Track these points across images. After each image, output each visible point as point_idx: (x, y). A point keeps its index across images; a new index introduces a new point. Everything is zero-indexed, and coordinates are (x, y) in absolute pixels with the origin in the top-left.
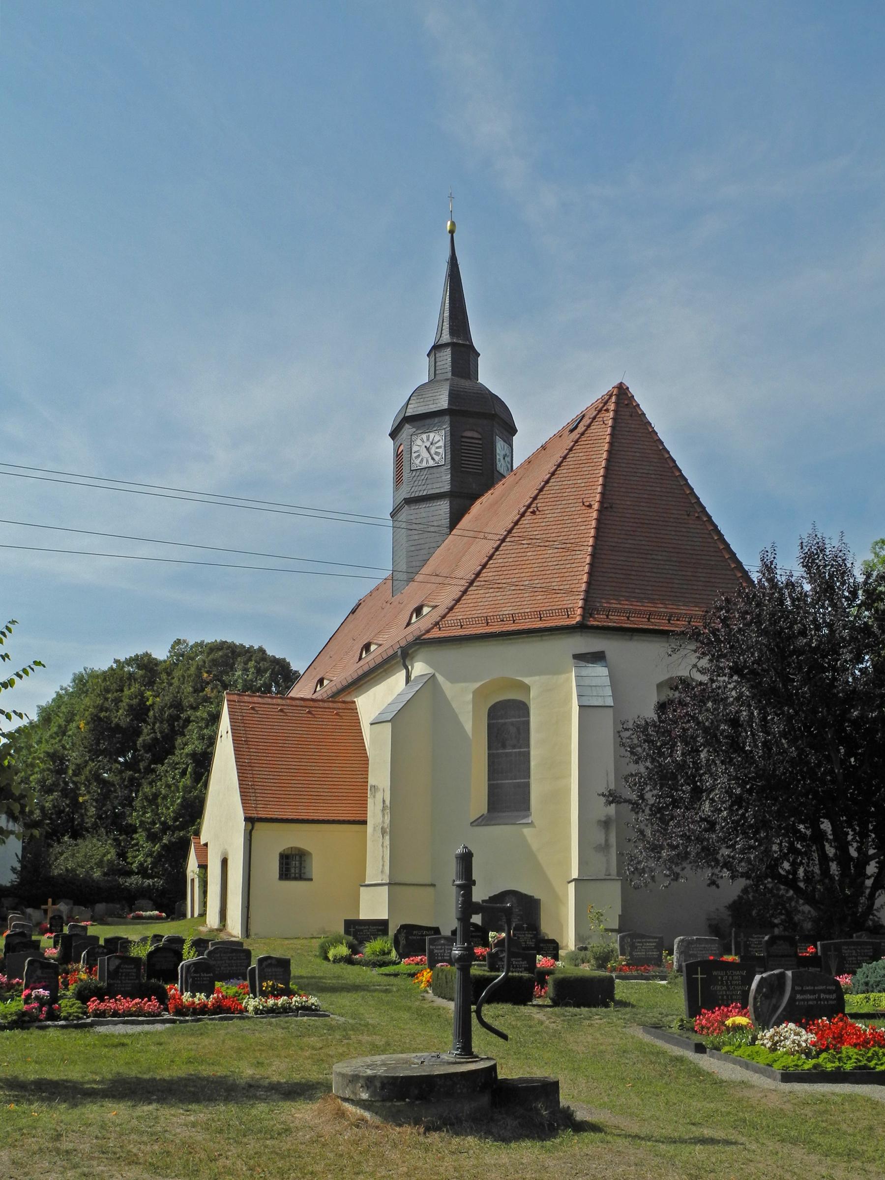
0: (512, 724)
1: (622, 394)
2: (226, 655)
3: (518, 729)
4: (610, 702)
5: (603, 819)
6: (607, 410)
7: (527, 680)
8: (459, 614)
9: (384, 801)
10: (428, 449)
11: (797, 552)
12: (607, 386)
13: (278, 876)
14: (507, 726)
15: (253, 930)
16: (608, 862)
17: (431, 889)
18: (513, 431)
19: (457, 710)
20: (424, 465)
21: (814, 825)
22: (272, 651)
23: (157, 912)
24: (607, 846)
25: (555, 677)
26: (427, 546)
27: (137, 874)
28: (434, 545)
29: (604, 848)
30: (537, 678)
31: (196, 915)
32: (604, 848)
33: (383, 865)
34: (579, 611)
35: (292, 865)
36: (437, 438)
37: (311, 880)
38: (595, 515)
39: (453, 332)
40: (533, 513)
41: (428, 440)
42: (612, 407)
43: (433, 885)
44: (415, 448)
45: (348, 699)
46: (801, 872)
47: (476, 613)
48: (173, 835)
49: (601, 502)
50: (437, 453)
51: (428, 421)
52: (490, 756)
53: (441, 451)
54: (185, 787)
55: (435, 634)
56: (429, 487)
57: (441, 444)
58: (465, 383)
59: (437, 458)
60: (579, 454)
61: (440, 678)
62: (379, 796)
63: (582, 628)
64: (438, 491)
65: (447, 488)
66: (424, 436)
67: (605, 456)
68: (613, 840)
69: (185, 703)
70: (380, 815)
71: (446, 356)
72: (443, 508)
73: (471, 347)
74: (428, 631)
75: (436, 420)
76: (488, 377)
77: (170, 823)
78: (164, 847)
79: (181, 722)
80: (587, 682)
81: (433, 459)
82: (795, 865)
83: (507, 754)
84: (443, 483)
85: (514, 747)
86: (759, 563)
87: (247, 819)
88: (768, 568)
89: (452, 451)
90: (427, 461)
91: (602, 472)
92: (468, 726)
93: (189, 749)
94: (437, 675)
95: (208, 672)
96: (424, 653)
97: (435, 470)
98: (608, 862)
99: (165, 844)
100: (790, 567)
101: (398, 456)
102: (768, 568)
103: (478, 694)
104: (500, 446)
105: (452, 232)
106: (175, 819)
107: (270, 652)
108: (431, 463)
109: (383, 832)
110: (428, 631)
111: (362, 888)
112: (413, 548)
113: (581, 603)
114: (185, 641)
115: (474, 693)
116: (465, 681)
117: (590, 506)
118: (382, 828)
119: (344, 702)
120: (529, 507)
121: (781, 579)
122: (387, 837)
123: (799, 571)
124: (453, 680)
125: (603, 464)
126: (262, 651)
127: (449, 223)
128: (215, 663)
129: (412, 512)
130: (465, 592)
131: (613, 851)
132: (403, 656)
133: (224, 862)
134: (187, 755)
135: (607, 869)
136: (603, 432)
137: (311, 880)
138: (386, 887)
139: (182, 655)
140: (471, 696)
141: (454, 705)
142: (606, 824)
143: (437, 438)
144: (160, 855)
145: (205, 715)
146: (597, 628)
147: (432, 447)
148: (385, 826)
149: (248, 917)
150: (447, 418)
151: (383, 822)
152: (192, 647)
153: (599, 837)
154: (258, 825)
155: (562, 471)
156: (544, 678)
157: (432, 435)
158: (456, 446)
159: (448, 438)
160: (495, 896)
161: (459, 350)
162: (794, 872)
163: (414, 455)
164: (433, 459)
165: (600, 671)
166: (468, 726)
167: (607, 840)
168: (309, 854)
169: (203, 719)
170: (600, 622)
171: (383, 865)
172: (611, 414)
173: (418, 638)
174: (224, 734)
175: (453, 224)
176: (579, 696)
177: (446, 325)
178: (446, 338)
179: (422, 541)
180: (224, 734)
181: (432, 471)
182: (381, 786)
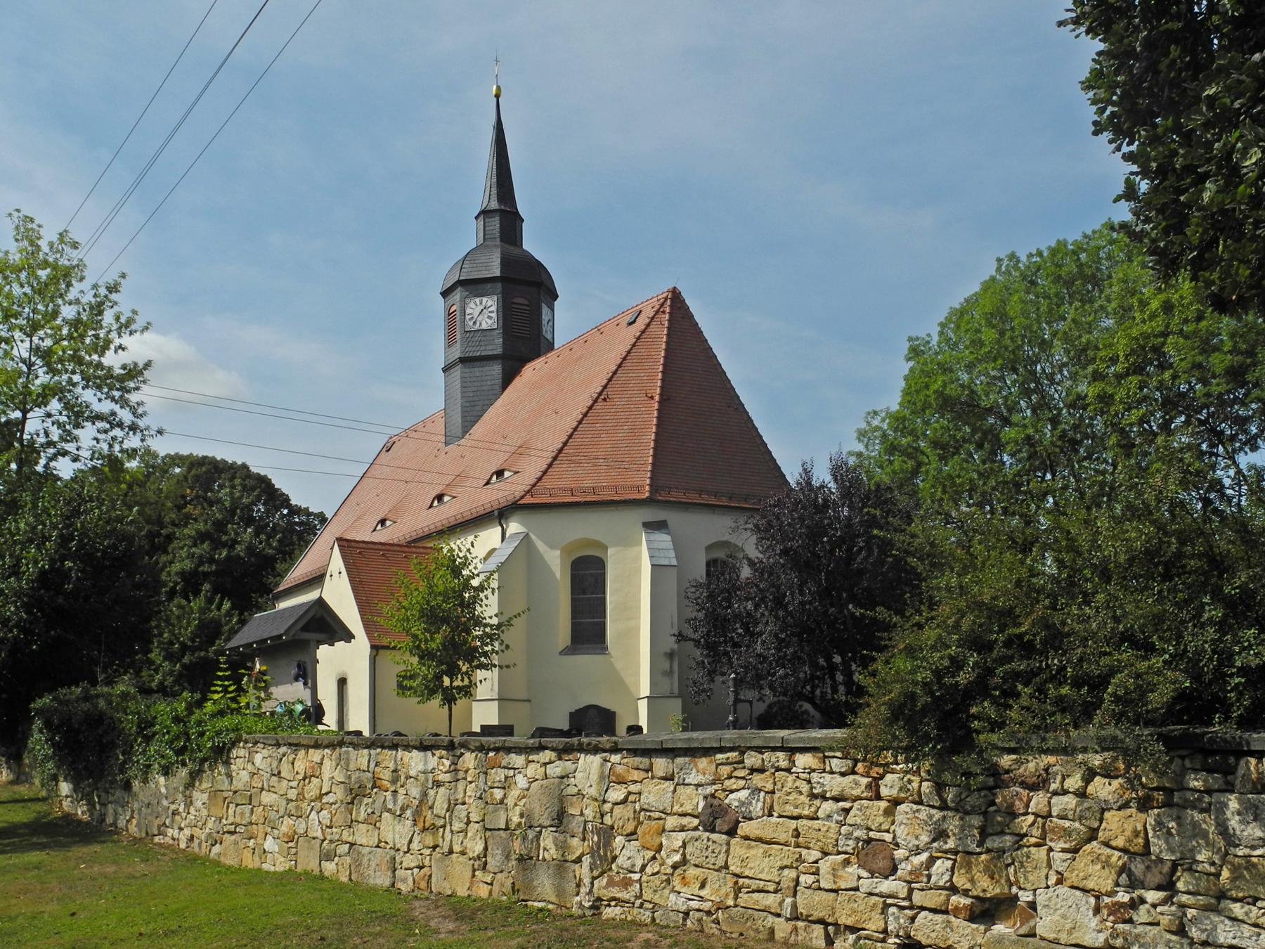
0: (591, 575)
1: (676, 298)
4: (674, 562)
6: (664, 312)
8: (547, 483)
11: (828, 465)
12: (661, 288)
14: (588, 577)
17: (527, 704)
18: (555, 296)
21: (829, 659)
24: (671, 672)
27: (157, 692)
34: (647, 488)
36: (490, 303)
38: (656, 406)
39: (501, 199)
40: (605, 400)
42: (668, 310)
43: (529, 701)
44: (468, 311)
46: (818, 692)
47: (561, 484)
49: (661, 394)
51: (481, 286)
52: (572, 599)
53: (494, 315)
54: (200, 608)
55: (528, 500)
57: (494, 308)
58: (512, 250)
60: (641, 350)
61: (533, 537)
63: (649, 502)
65: (499, 351)
66: (477, 300)
67: (663, 354)
68: (676, 667)
69: (167, 519)
71: (495, 223)
72: (496, 370)
73: (517, 214)
75: (489, 286)
76: (531, 244)
77: (189, 643)
78: (184, 666)
79: (162, 539)
80: (655, 545)
82: (814, 687)
84: (496, 346)
86: (801, 470)
87: (372, 647)
88: (807, 472)
89: (504, 312)
91: (661, 368)
92: (558, 575)
93: (177, 567)
100: (822, 475)
101: (450, 315)
102: (807, 472)
104: (545, 309)
105: (497, 96)
107: (254, 470)
110: (522, 497)
113: (648, 481)
117: (652, 398)
120: (600, 394)
121: (816, 483)
123: (828, 478)
125: (662, 361)
126: (245, 467)
128: (197, 478)
130: (550, 465)
131: (676, 676)
132: (500, 515)
133: (342, 682)
134: (177, 574)
136: (661, 332)
142: (671, 655)
143: (490, 303)
144: (180, 675)
146: (667, 502)
147: (484, 312)
150: (499, 285)
154: (381, 652)
155: (627, 364)
157: (485, 299)
158: (507, 311)
161: (505, 217)
162: (813, 692)
163: (468, 317)
165: (663, 539)
166: (558, 575)
170: (665, 497)
172: (667, 316)
173: (515, 503)
174: (336, 575)
175: (499, 88)
176: (651, 557)
177: (494, 191)
178: (494, 205)
180: (336, 575)
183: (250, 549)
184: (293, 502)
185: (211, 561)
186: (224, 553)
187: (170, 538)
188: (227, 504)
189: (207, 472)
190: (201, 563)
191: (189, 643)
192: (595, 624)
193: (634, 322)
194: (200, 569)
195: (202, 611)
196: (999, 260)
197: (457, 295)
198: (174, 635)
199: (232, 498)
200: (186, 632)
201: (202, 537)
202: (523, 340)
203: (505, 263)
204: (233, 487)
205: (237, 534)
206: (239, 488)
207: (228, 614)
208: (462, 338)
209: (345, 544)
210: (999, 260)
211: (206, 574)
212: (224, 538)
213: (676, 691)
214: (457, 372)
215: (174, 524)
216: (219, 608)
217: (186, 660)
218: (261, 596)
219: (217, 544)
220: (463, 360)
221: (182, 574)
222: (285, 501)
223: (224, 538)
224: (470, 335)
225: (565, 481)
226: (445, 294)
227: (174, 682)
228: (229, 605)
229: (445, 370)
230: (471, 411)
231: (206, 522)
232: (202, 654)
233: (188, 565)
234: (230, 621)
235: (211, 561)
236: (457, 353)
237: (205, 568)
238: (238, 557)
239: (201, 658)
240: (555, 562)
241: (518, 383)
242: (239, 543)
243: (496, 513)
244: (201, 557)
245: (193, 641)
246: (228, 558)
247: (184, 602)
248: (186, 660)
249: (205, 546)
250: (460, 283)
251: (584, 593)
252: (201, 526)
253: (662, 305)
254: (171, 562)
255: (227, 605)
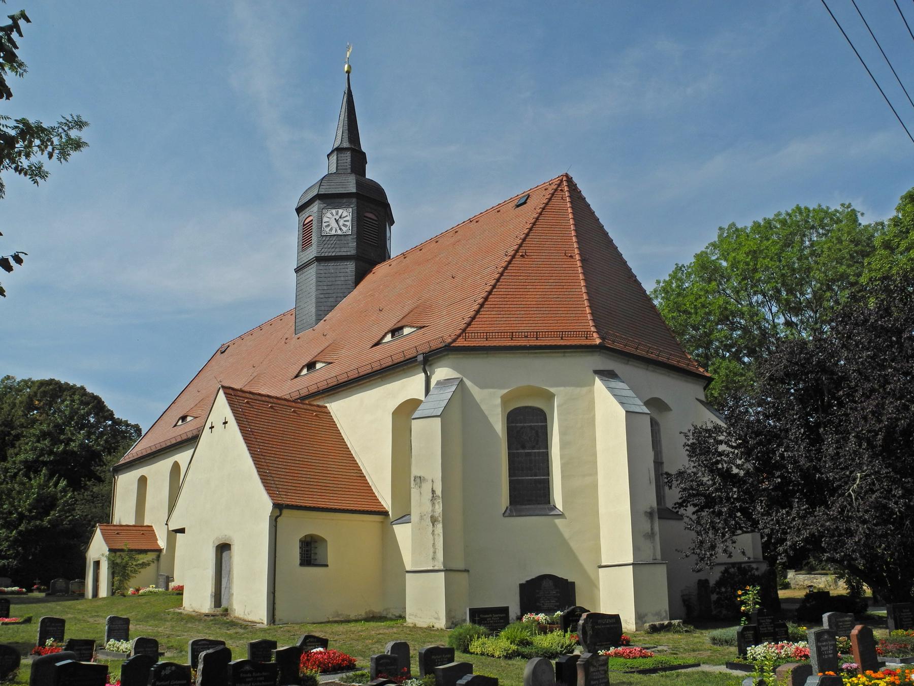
2: (55, 389)
3: (537, 433)
5: (649, 510)
7: (552, 390)
9: (433, 492)
10: (337, 221)
13: (298, 562)
14: (528, 433)
15: (279, 615)
16: (654, 548)
17: (466, 574)
19: (486, 413)
20: (333, 233)
22: (90, 389)
23: (16, 588)
25: (579, 389)
26: (334, 295)
28: (341, 295)
29: (651, 536)
30: (562, 388)
31: (103, 592)
32: (651, 536)
33: (435, 553)
35: (311, 550)
37: (327, 566)
41: (337, 214)
43: (467, 571)
44: (325, 219)
45: (320, 403)
48: (29, 523)
50: (344, 225)
53: (349, 224)
55: (460, 343)
56: (337, 250)
57: (349, 218)
59: (344, 229)
61: (468, 383)
62: (427, 487)
64: (344, 254)
65: (353, 252)
66: (334, 211)
68: (657, 529)
70: (429, 504)
71: (347, 157)
72: (351, 267)
74: (454, 341)
75: (345, 200)
77: (27, 513)
78: (20, 533)
81: (340, 229)
83: (529, 454)
84: (351, 248)
85: (533, 448)
90: (336, 231)
93: (22, 457)
94: (465, 379)
95: (40, 401)
96: (451, 359)
97: (342, 238)
98: (654, 548)
99: (21, 531)
103: (505, 400)
106: (30, 511)
108: (339, 232)
109: (434, 520)
110: (454, 341)
111: (407, 574)
112: (322, 296)
114: (13, 378)
115: (502, 397)
116: (493, 387)
118: (432, 517)
119: (318, 406)
120: (517, 251)
122: (439, 528)
124: (482, 386)
126: (82, 388)
127: (346, 66)
128: (45, 394)
129: (321, 268)
131: (657, 538)
132: (427, 360)
134: (21, 462)
135: (654, 555)
137: (327, 566)
138: (443, 573)
139: (10, 388)
140: (499, 400)
141: (483, 407)
145: (37, 432)
147: (340, 221)
148: (436, 514)
149: (274, 603)
150: (354, 200)
151: (433, 511)
152: (19, 383)
153: (646, 526)
154: (286, 512)
156: (569, 389)
157: (340, 211)
158: (360, 221)
159: (355, 215)
160: (532, 580)
163: (324, 225)
164: (340, 229)
167: (652, 529)
168: (323, 541)
169: (34, 435)
171: (435, 553)
174: (219, 426)
175: (350, 67)
178: (346, 145)
179: (331, 291)
180: (219, 426)
181: (340, 238)
182: (429, 477)
183: (82, 445)
184: (116, 416)
185: (51, 452)
186: (62, 447)
187: (18, 437)
188: (67, 413)
189: (53, 391)
190: (42, 455)
191: (27, 513)
192: (540, 481)
193: (525, 203)
194: (41, 459)
195: (40, 487)
196: (721, 229)
197: (315, 208)
198: (14, 506)
199: (72, 408)
200: (25, 504)
201: (44, 435)
202: (370, 247)
203: (359, 184)
204: (73, 401)
205: (73, 434)
206: (77, 402)
207: (64, 490)
208: (319, 242)
209: (231, 392)
210: (721, 229)
211: (45, 463)
212: (62, 437)
213: (659, 557)
214: (312, 272)
215: (22, 426)
216: (56, 485)
217: (22, 528)
218: (89, 480)
219: (55, 441)
220: (319, 259)
221: (25, 462)
222: (111, 415)
223: (62, 437)
224: (325, 239)
225: (494, 326)
226: (299, 210)
227: (9, 546)
228: (65, 482)
229: (297, 271)
230: (326, 305)
231: (49, 425)
232: (38, 522)
233: (31, 456)
234: (65, 496)
235: (51, 452)
236: (312, 252)
237: (46, 458)
238: (73, 452)
239: (36, 526)
240: (493, 408)
241: (369, 278)
242: (74, 441)
243: (420, 358)
244: (42, 449)
245: (30, 511)
246: (64, 451)
247: (26, 480)
248: (22, 528)
249: (46, 442)
250: (319, 197)
251: (524, 447)
252: (44, 427)
253: (559, 185)
254: (16, 454)
255: (63, 483)
